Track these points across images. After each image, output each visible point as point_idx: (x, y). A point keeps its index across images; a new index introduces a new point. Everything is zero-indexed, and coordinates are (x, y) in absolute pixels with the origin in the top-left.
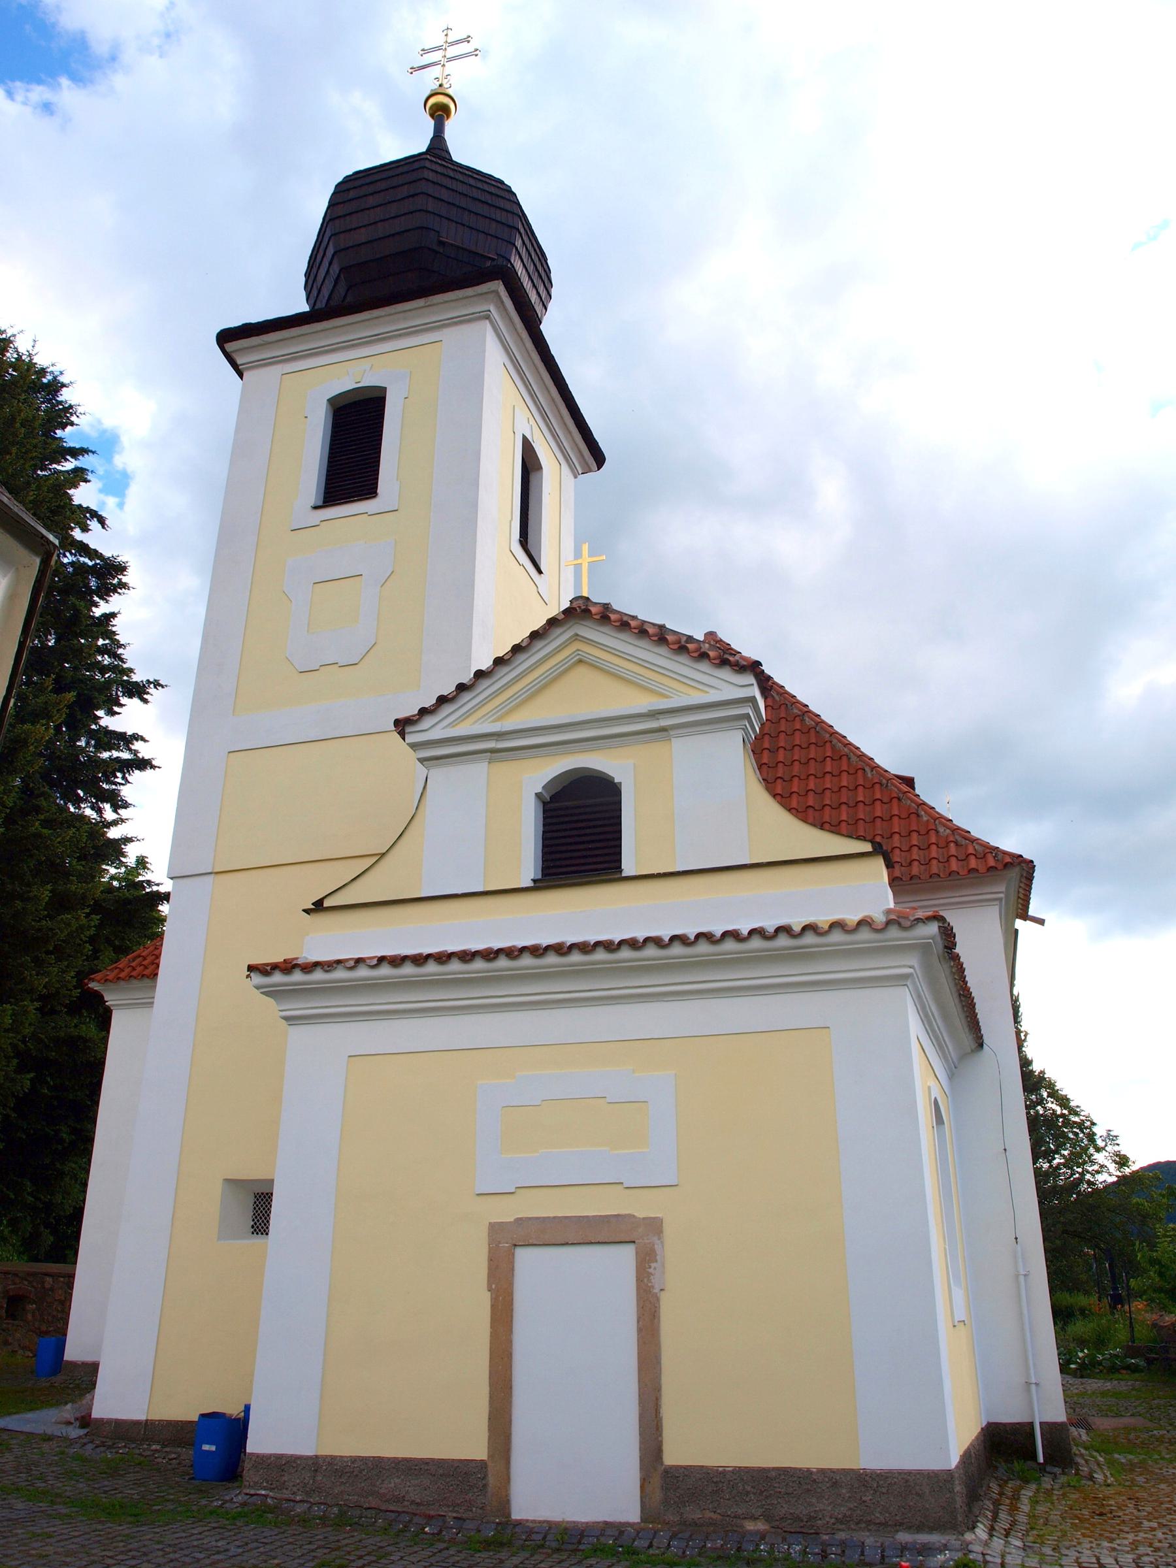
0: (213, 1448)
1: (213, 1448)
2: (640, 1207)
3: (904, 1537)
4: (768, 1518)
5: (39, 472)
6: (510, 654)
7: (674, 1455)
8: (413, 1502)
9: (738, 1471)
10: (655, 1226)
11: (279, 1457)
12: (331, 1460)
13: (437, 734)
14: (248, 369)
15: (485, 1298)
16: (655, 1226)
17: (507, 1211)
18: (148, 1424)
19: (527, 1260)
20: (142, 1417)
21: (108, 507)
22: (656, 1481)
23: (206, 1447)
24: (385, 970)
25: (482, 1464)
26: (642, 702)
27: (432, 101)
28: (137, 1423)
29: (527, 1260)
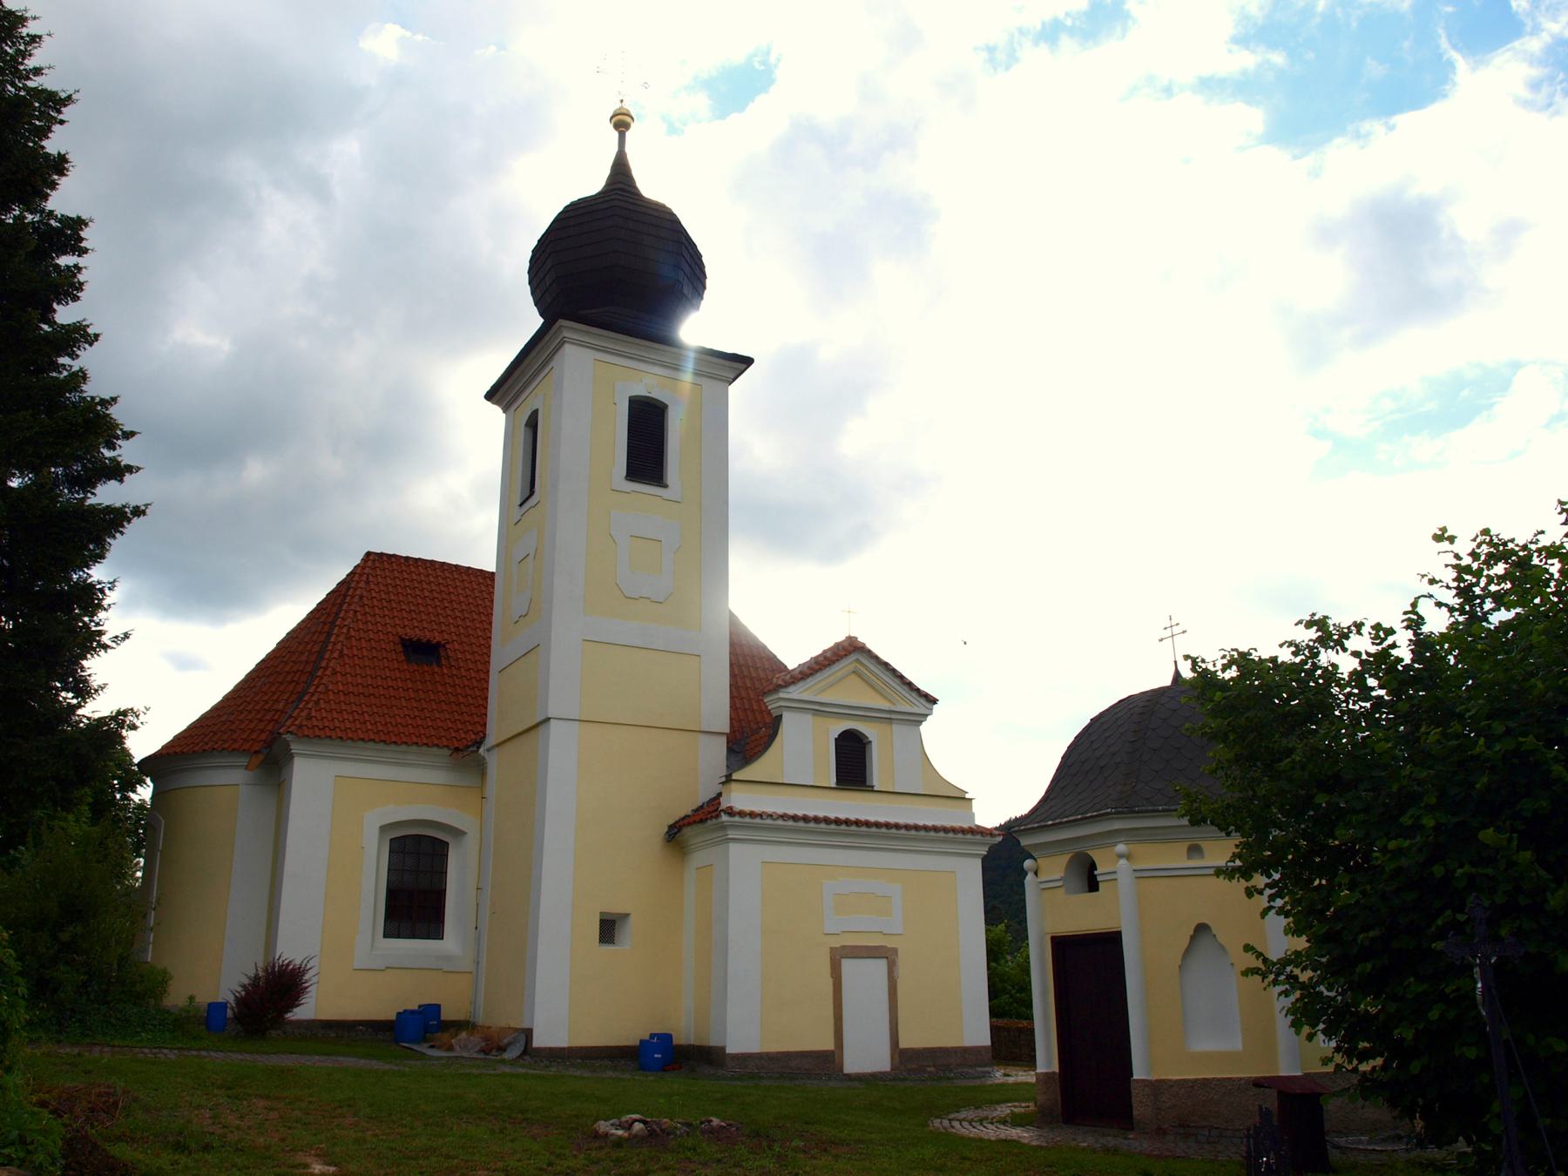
0: (660, 1056)
1: (660, 1056)
2: (889, 943)
3: (979, 1069)
4: (934, 1066)
5: (1300, 908)
6: (1212, 871)
7: (903, 1044)
8: (806, 1069)
9: (924, 1049)
10: (895, 951)
11: (743, 1054)
12: (768, 1055)
13: (795, 696)
14: (568, 342)
15: (830, 981)
16: (895, 951)
17: (837, 943)
18: (570, 1049)
19: (882, 965)
20: (566, 1045)
21: (71, 168)
22: (897, 1056)
23: (656, 1056)
24: (790, 823)
25: (832, 1052)
26: (883, 704)
27: (613, 120)
28: (563, 1049)
29: (882, 965)
